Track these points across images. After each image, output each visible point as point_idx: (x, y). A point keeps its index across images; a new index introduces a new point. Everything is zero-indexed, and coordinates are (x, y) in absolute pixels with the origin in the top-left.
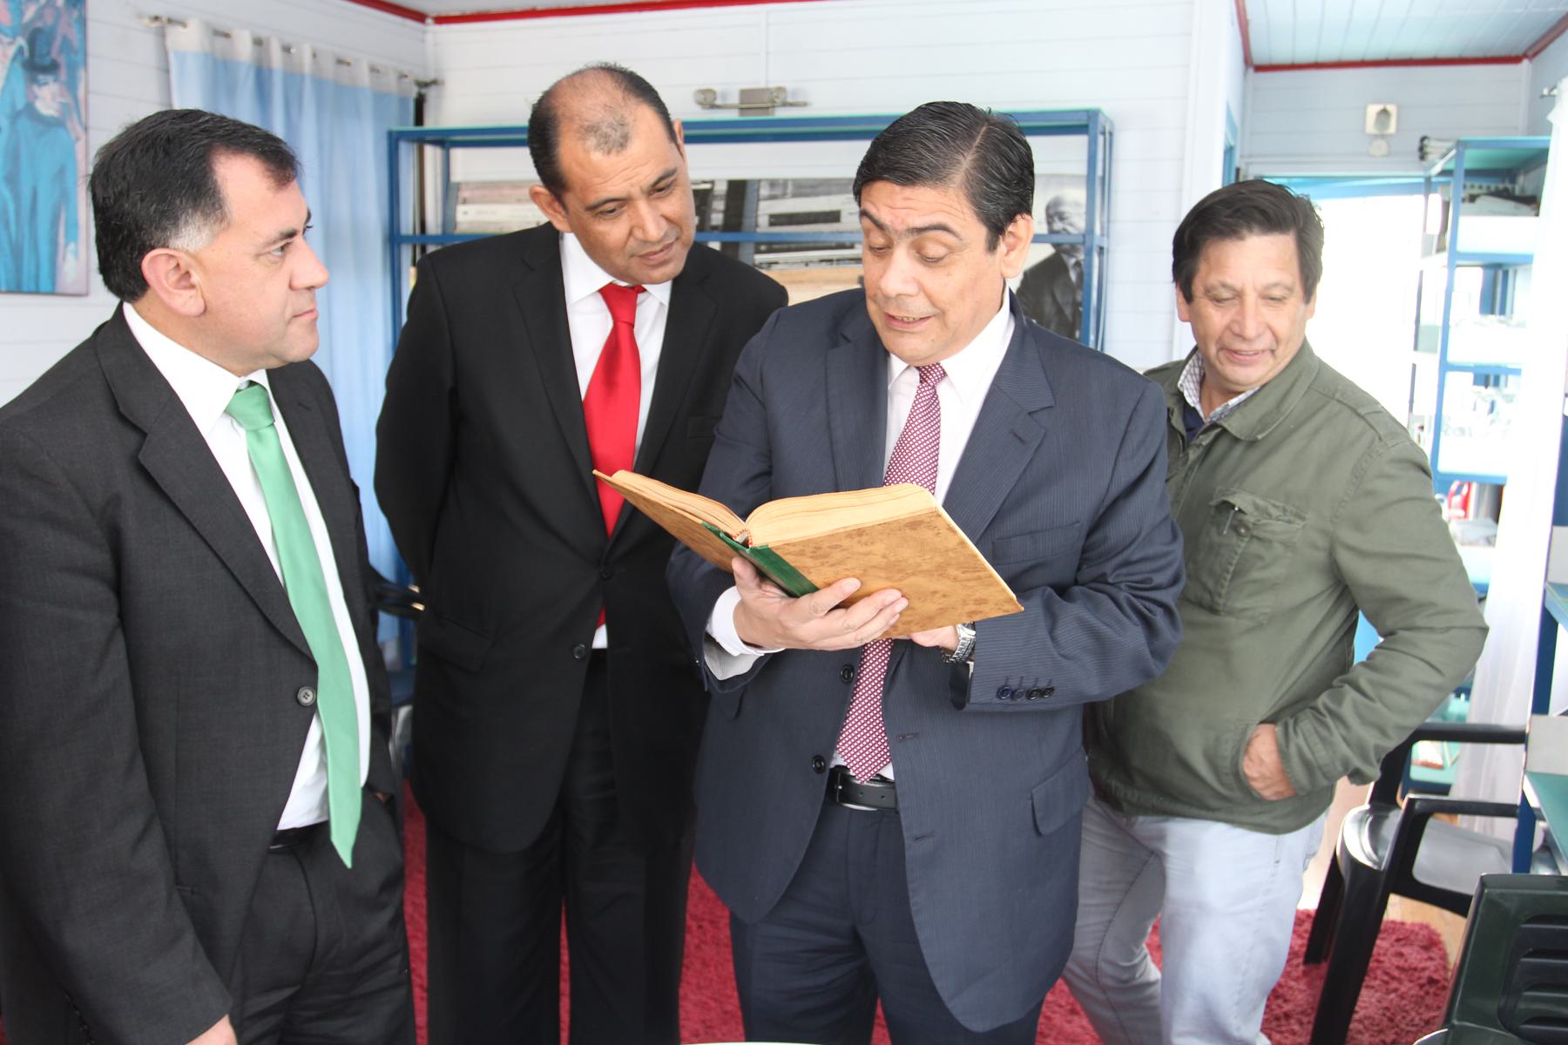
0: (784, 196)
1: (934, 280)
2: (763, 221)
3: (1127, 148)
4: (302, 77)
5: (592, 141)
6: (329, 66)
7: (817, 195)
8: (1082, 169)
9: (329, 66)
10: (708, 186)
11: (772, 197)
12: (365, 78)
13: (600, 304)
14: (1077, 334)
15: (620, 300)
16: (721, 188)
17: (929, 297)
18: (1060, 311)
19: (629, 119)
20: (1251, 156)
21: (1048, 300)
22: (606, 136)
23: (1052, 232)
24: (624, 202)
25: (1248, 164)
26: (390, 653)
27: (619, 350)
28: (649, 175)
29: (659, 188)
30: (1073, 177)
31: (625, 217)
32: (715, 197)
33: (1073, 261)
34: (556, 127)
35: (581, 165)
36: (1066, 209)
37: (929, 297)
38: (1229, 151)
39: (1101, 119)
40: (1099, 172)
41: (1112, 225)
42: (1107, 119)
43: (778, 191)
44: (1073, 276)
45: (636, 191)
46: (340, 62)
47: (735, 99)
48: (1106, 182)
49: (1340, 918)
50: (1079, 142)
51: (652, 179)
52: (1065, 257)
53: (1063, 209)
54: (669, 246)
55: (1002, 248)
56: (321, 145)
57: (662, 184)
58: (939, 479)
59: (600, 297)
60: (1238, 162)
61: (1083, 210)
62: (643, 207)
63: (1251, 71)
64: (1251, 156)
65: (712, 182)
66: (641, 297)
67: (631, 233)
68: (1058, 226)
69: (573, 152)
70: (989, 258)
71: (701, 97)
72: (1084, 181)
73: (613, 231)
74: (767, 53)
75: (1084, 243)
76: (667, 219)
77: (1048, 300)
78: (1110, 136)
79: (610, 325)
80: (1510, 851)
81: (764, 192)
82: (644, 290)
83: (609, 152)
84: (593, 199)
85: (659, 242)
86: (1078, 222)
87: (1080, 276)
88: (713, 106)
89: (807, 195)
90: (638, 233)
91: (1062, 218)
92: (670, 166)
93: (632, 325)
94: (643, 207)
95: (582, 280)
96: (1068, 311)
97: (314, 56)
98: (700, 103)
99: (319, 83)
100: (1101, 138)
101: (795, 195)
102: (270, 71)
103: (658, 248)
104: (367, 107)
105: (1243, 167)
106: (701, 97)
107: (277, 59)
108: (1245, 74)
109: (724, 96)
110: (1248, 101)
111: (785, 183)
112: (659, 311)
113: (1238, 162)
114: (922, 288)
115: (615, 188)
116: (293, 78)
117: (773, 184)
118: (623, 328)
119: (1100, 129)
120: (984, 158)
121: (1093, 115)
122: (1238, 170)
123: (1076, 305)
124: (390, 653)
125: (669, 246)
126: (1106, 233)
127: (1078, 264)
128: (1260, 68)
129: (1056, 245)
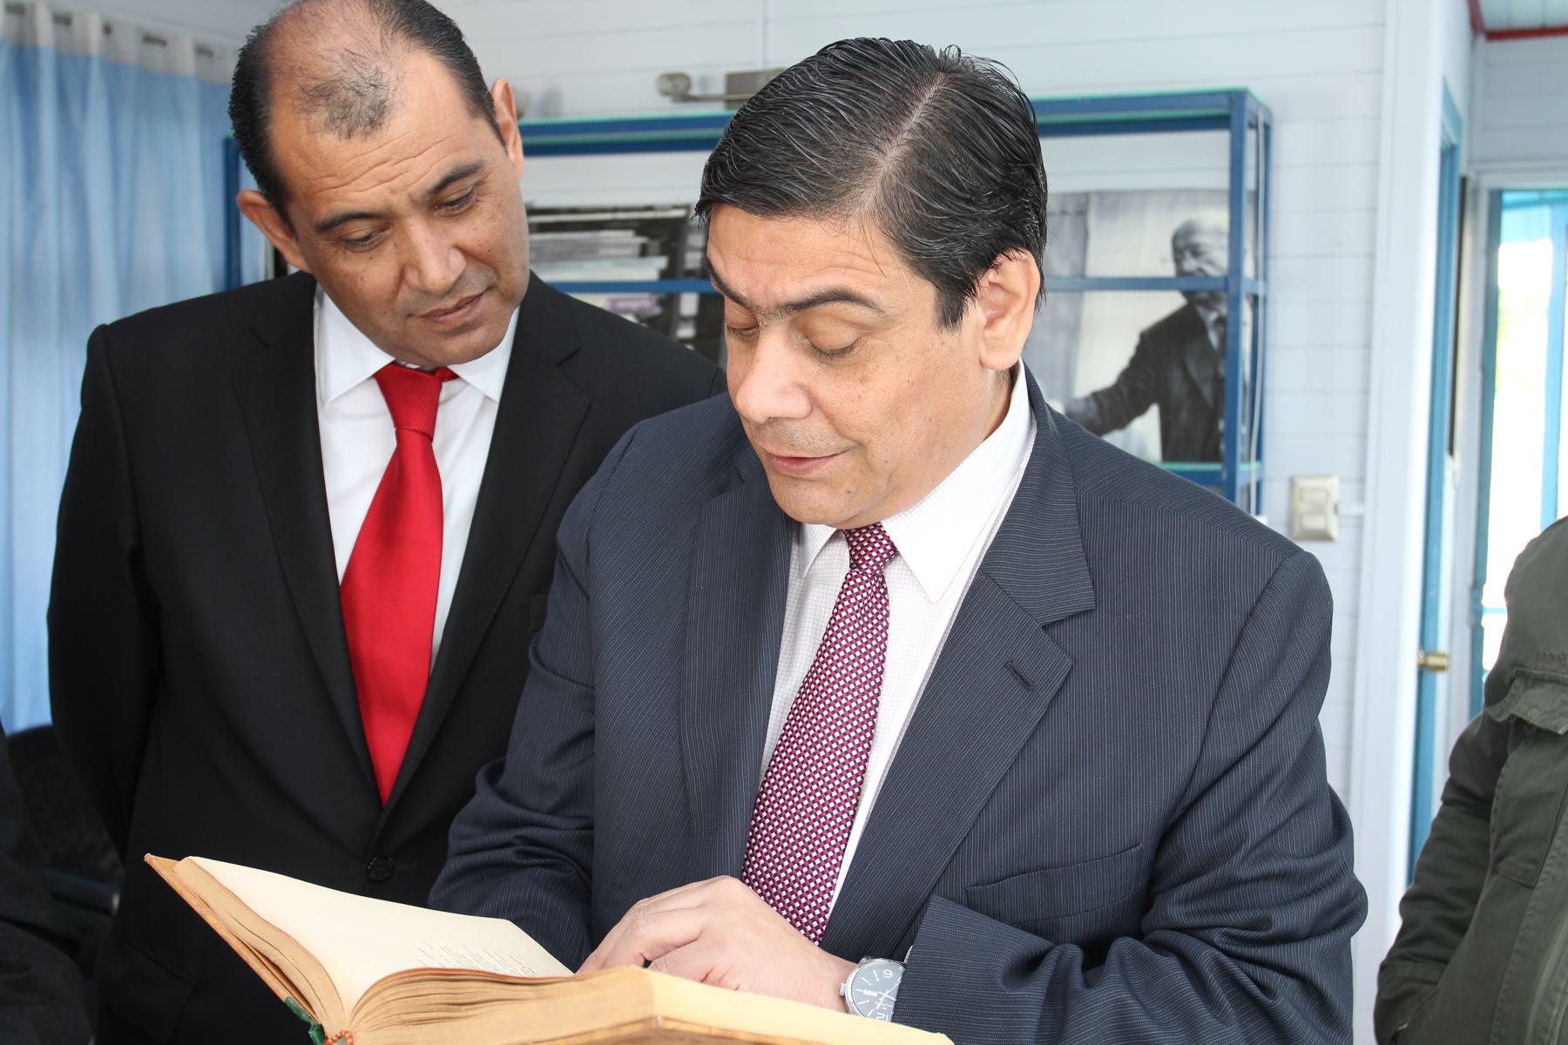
1: (833, 388)
3: (1291, 143)
4: (88, 59)
5: (321, 115)
6: (129, 47)
8: (1222, 180)
9: (129, 47)
10: (680, 213)
12: (187, 62)
13: (375, 400)
14: (1221, 425)
15: (411, 391)
17: (830, 418)
18: (1195, 391)
19: (389, 75)
20: (1482, 161)
21: (1176, 375)
22: (347, 105)
23: (1181, 273)
24: (384, 221)
25: (1479, 173)
27: (407, 487)
28: (427, 171)
29: (448, 198)
30: (1212, 192)
31: (389, 247)
32: (690, 229)
33: (1213, 316)
34: (267, 89)
35: (303, 155)
36: (1201, 239)
37: (830, 418)
38: (1448, 154)
39: (1249, 104)
40: (1249, 183)
41: (1272, 263)
42: (1259, 104)
44: (1213, 338)
45: (400, 202)
46: (149, 39)
47: (719, 88)
48: (1262, 198)
50: (1219, 140)
51: (432, 178)
52: (1201, 310)
54: (475, 299)
55: (975, 313)
56: (115, 158)
57: (452, 193)
59: (374, 383)
60: (1463, 168)
61: (1225, 241)
62: (419, 231)
63: (1482, 39)
64: (1482, 161)
66: (448, 387)
67: (401, 277)
68: (1190, 264)
69: (297, 134)
70: (949, 338)
71: (668, 85)
72: (1225, 198)
73: (373, 273)
74: (766, 21)
75: (1226, 289)
76: (466, 253)
77: (1176, 375)
78: (1267, 135)
79: (392, 444)
82: (454, 376)
83: (349, 135)
84: (325, 212)
85: (450, 291)
86: (1219, 258)
87: (1223, 339)
88: (686, 98)
90: (412, 277)
91: (1196, 252)
92: (467, 157)
93: (429, 437)
94: (419, 231)
95: (346, 363)
96: (1207, 391)
97: (107, 30)
98: (665, 93)
99: (113, 68)
100: (1250, 136)
102: (36, 51)
103: (450, 303)
104: (191, 106)
105: (1472, 176)
106: (668, 85)
107: (45, 31)
108: (1473, 44)
109: (704, 82)
110: (1475, 76)
112: (483, 408)
113: (1463, 168)
114: (815, 403)
115: (364, 195)
116: (71, 64)
118: (414, 441)
119: (1248, 118)
121: (1237, 98)
122: (1464, 181)
123: (1219, 382)
125: (475, 299)
126: (1263, 273)
127: (1221, 321)
128: (1496, 35)
129: (1187, 294)
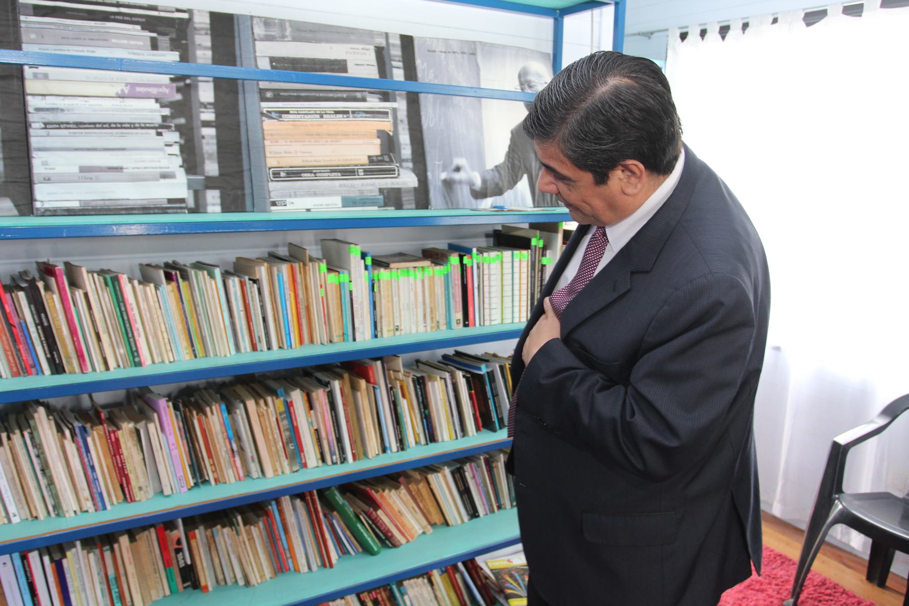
0: (283, 37)
2: (264, 64)
7: (319, 41)
10: (185, 16)
11: (269, 38)
16: (202, 20)
26: (290, 561)
43: (275, 32)
49: (780, 483)
53: (531, 78)
58: (602, 260)
65: (190, 12)
80: (867, 564)
81: (259, 30)
83: (577, 137)
89: (308, 40)
101: (295, 39)
111: (282, 23)
117: (267, 22)
120: (664, 155)
124: (290, 561)
